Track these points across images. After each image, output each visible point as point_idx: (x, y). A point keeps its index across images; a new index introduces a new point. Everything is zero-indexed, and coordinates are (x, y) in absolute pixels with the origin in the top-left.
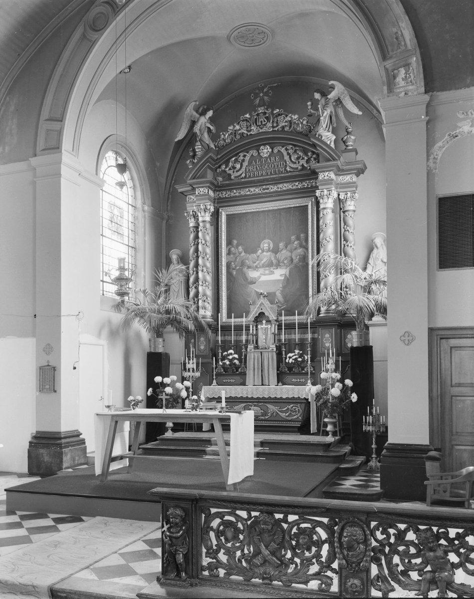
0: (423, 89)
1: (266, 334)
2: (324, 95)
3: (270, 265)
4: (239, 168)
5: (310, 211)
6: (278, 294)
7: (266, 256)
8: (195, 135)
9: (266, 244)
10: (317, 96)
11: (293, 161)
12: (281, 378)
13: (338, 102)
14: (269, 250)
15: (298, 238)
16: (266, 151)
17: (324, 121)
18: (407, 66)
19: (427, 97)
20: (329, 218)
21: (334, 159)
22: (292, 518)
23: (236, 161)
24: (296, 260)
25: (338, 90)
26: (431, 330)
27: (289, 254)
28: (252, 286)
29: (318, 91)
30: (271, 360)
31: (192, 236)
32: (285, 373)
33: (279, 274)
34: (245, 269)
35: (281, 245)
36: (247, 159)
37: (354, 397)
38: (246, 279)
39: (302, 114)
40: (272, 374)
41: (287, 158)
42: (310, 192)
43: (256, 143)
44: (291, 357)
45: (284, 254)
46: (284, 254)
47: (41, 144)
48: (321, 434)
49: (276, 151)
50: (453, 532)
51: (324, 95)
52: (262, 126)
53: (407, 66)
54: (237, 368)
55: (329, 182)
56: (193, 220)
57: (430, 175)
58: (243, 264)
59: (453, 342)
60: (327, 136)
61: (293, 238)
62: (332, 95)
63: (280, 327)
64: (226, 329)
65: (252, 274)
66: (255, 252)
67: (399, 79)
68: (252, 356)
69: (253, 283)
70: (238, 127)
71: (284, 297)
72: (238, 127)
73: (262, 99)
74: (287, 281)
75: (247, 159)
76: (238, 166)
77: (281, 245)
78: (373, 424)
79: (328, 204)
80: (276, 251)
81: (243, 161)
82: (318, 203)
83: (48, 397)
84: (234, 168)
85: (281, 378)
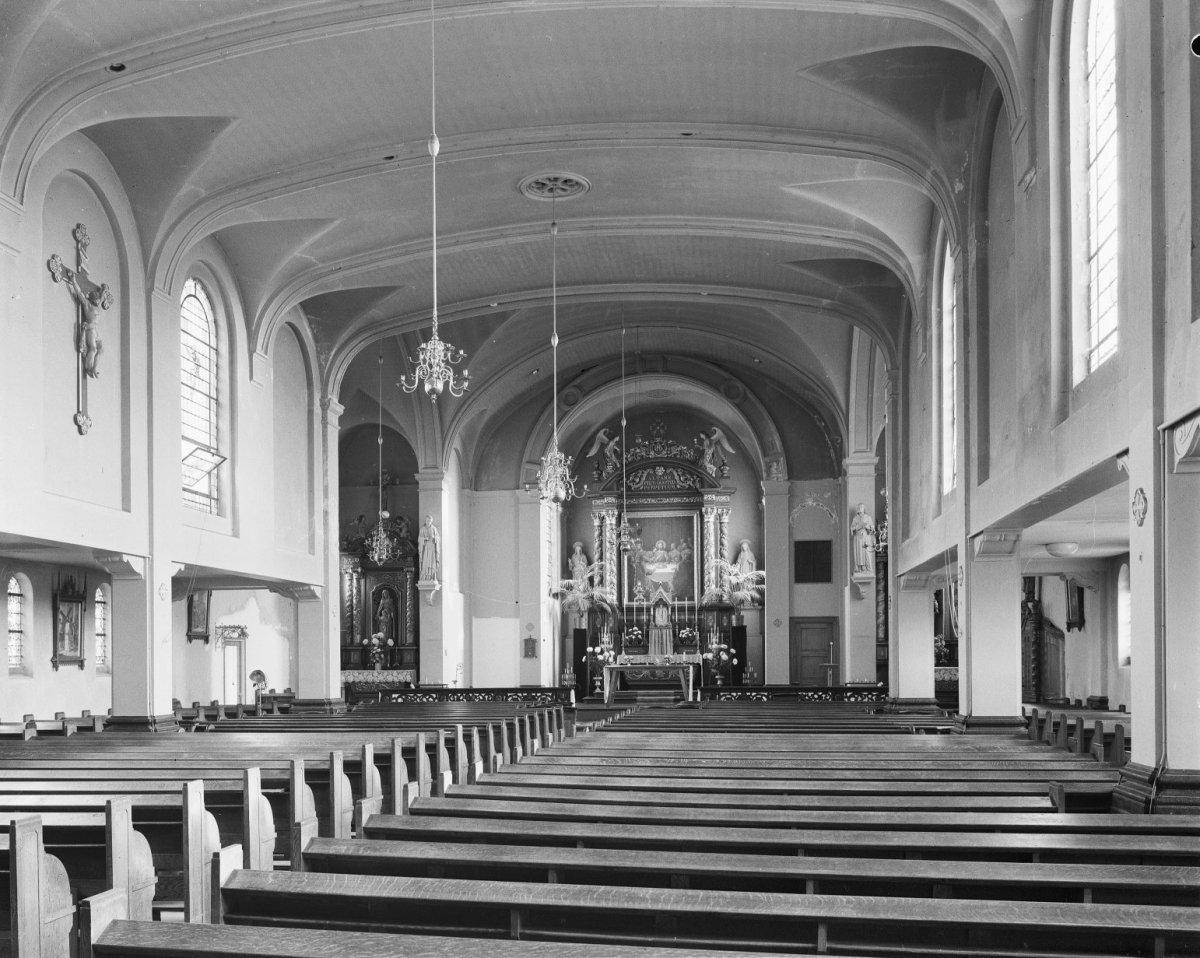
0: (786, 478)
1: (661, 617)
2: (708, 436)
3: (663, 560)
4: (641, 481)
5: (695, 521)
6: (670, 584)
7: (660, 554)
8: (605, 455)
9: (660, 544)
10: (703, 436)
11: (679, 480)
12: (677, 649)
13: (718, 442)
14: (662, 549)
15: (686, 541)
16: (660, 471)
17: (708, 457)
18: (778, 462)
19: (788, 484)
20: (711, 528)
21: (716, 487)
22: (753, 694)
23: (635, 476)
24: (684, 557)
25: (718, 434)
26: (791, 618)
27: (678, 553)
28: (649, 577)
29: (703, 433)
30: (668, 635)
31: (597, 533)
32: (679, 645)
33: (671, 569)
34: (643, 563)
35: (672, 545)
36: (645, 475)
37: (735, 661)
38: (643, 571)
39: (690, 446)
40: (670, 649)
41: (677, 478)
42: (698, 506)
43: (653, 464)
44: (684, 633)
45: (675, 553)
46: (675, 553)
47: (522, 479)
48: (229, 916)
49: (668, 471)
50: (810, 694)
51: (708, 436)
52: (658, 452)
53: (778, 462)
54: (639, 641)
55: (712, 502)
56: (598, 520)
57: (790, 528)
58: (641, 558)
59: (803, 625)
60: (711, 469)
61: (682, 540)
62: (714, 437)
63: (673, 609)
64: (630, 610)
65: (649, 567)
66: (651, 549)
67: (773, 469)
68: (653, 633)
69: (648, 574)
70: (638, 451)
71: (675, 587)
72: (638, 451)
73: (658, 431)
74: (677, 574)
75: (645, 475)
76: (638, 480)
77: (672, 545)
78: (750, 679)
79: (710, 519)
80: (668, 550)
81: (642, 476)
82: (702, 517)
83: (529, 662)
84: (634, 481)
85: (677, 649)
